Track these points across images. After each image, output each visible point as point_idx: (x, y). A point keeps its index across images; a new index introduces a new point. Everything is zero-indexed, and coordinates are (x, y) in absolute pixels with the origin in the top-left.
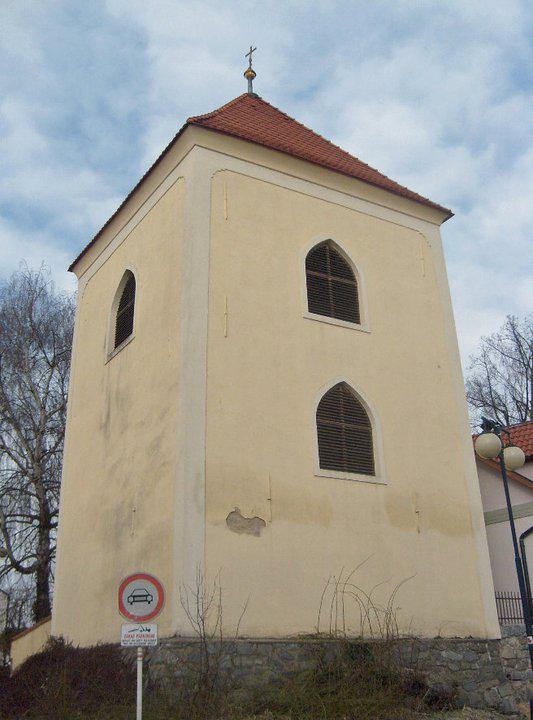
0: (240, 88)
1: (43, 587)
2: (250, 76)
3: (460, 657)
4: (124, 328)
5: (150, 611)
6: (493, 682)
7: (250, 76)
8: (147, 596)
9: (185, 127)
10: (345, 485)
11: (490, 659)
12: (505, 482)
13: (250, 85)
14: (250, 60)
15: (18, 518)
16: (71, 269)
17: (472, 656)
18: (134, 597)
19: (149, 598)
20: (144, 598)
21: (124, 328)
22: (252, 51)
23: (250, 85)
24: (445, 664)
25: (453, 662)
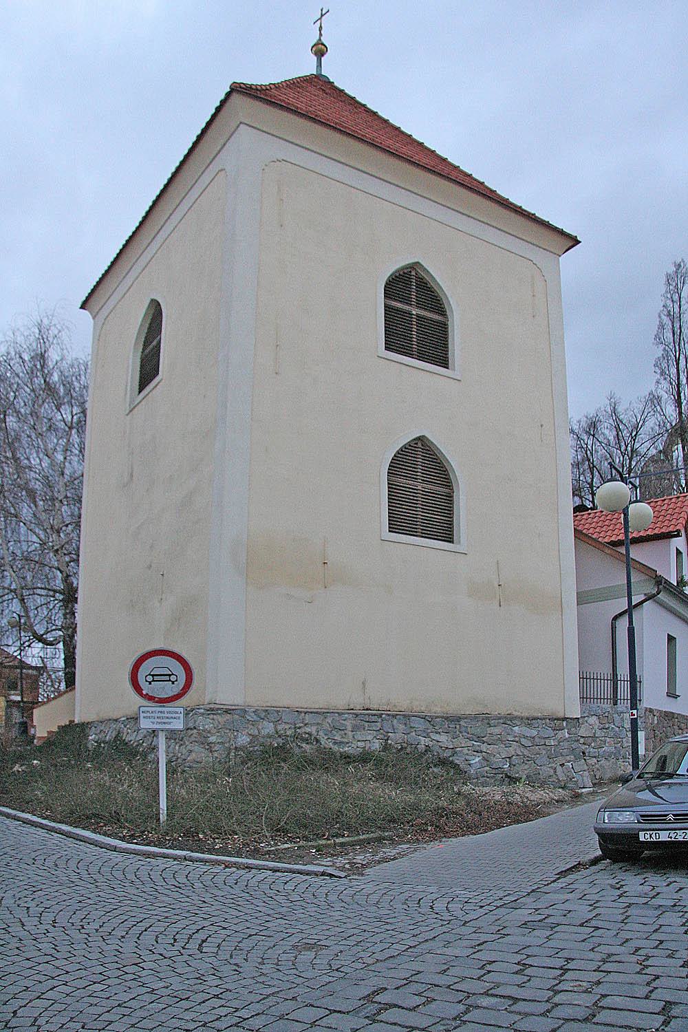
0: (308, 67)
1: (70, 660)
2: (320, 51)
3: (534, 733)
4: (148, 371)
5: (171, 694)
6: (568, 758)
7: (320, 51)
8: (170, 675)
9: (228, 95)
10: (543, 423)
11: (567, 736)
12: (628, 565)
13: (319, 65)
14: (321, 28)
15: (39, 591)
16: (83, 307)
17: (550, 732)
18: (153, 675)
19: (173, 678)
20: (168, 677)
21: (148, 371)
22: (322, 15)
23: (319, 65)
24: (517, 739)
25: (526, 737)
